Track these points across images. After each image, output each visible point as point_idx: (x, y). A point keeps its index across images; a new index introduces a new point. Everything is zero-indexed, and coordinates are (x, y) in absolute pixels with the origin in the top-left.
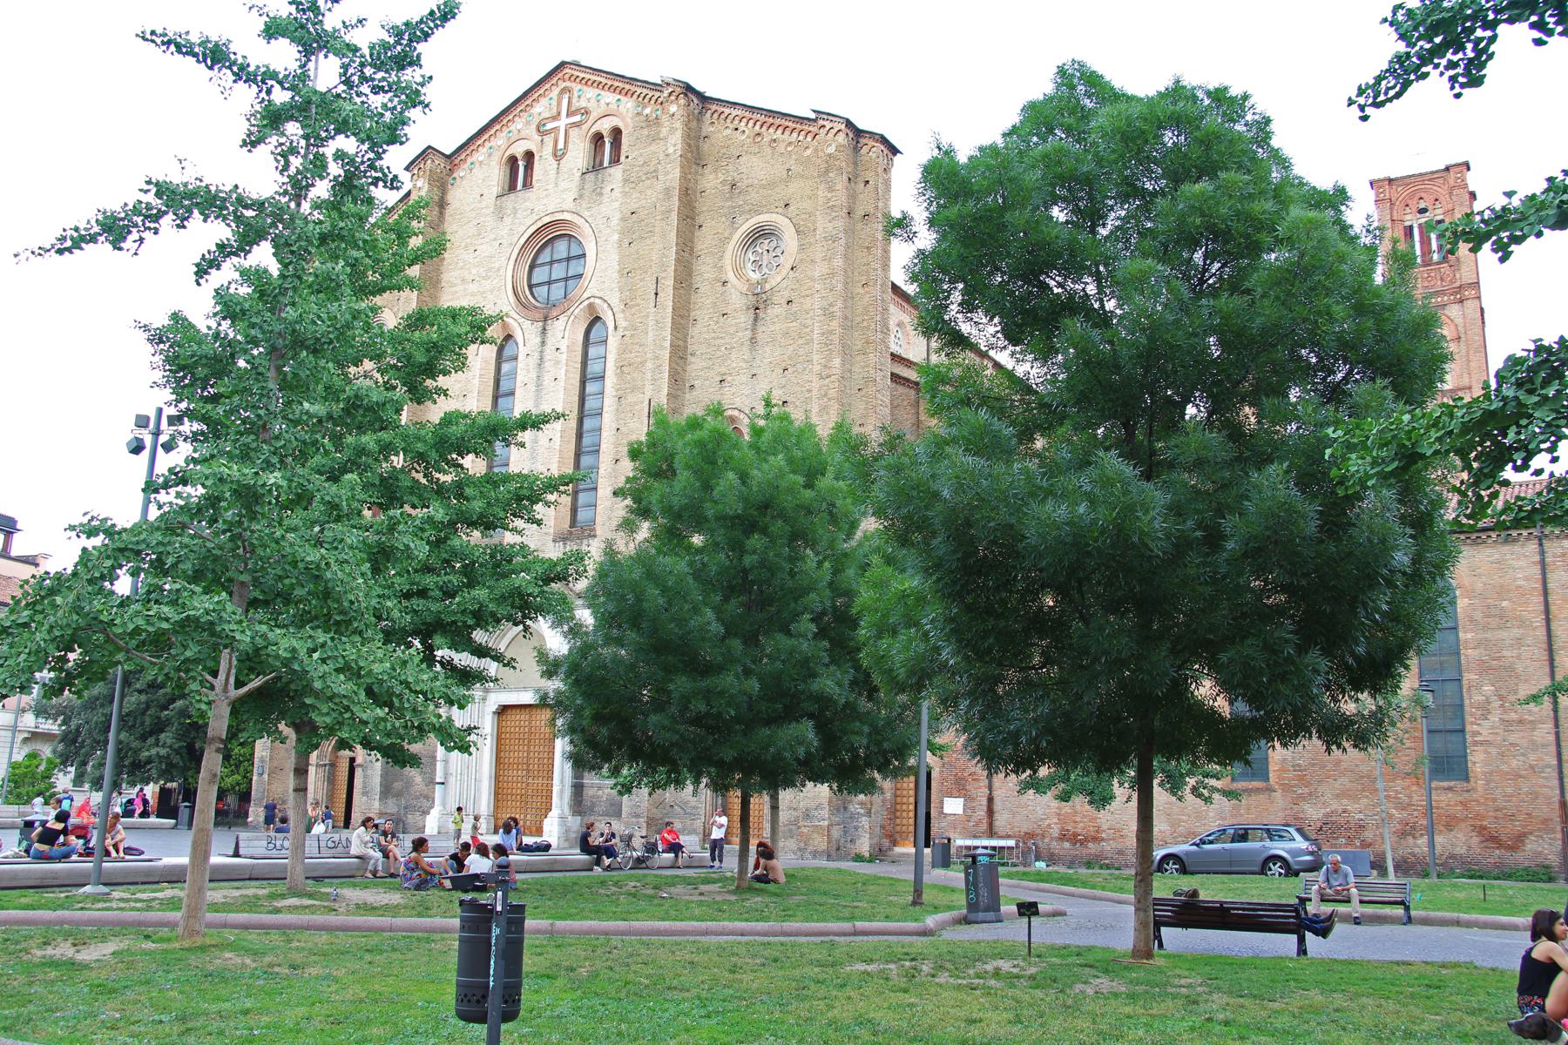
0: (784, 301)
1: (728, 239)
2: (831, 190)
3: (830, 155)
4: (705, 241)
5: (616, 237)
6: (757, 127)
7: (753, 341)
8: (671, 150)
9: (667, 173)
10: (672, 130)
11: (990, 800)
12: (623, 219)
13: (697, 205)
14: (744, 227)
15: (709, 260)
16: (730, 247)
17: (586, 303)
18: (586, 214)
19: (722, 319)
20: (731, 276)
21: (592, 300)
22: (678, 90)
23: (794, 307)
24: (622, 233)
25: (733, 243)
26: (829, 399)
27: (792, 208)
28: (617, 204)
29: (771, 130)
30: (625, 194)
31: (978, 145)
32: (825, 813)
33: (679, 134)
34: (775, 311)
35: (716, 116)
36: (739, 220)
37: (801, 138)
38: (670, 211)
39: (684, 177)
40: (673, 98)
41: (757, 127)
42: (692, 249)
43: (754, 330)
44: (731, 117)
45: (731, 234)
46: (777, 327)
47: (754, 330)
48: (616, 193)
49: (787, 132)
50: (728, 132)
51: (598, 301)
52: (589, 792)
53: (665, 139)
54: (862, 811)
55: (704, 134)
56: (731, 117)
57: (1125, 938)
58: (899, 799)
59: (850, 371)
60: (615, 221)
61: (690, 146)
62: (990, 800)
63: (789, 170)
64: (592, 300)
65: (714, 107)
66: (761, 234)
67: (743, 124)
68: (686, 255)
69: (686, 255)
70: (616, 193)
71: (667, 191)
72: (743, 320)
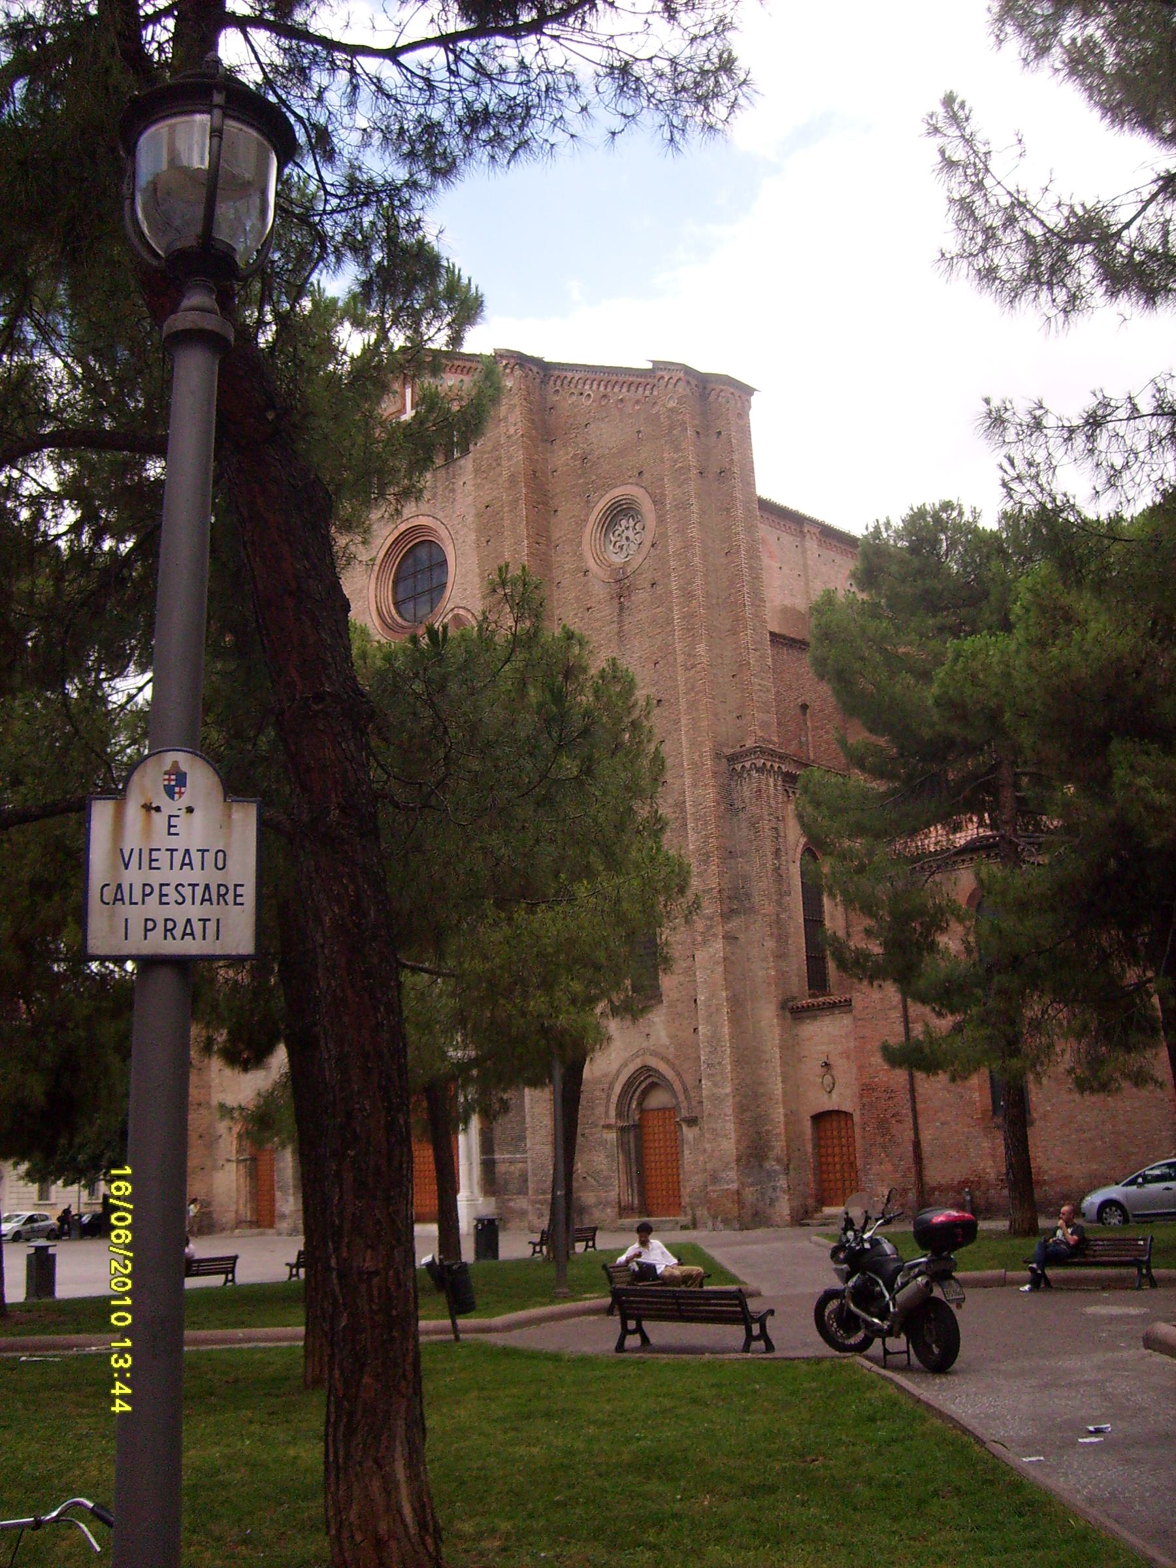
0: (647, 585)
1: (586, 521)
2: (677, 449)
3: (672, 410)
4: (561, 529)
5: (473, 536)
6: (602, 388)
7: (620, 634)
8: (512, 431)
9: (510, 458)
10: (512, 408)
11: (917, 1144)
12: (479, 515)
13: (549, 487)
14: (600, 505)
15: (568, 548)
16: (588, 530)
17: (450, 616)
18: (440, 515)
19: (587, 614)
20: (591, 564)
21: (456, 612)
22: (512, 361)
23: (659, 590)
24: (478, 531)
25: (590, 524)
26: (697, 693)
27: (645, 476)
28: (470, 499)
29: (616, 389)
30: (478, 487)
31: (526, 169)
32: (732, 1174)
33: (518, 410)
34: (641, 596)
35: (559, 383)
36: (594, 497)
37: (647, 393)
38: (518, 500)
39: (530, 459)
40: (508, 371)
41: (602, 388)
42: (548, 539)
43: (621, 622)
44: (574, 381)
45: (587, 515)
46: (643, 615)
47: (621, 622)
48: (469, 487)
49: (633, 388)
50: (574, 398)
51: (461, 612)
52: (501, 1168)
53: (506, 418)
54: (777, 1167)
55: (549, 405)
56: (574, 381)
57: (741, 1342)
58: (823, 1151)
59: (721, 656)
60: (470, 519)
61: (532, 421)
62: (917, 1144)
63: (639, 432)
64: (456, 612)
65: (556, 373)
66: (621, 511)
67: (587, 387)
68: (543, 547)
69: (543, 547)
70: (469, 487)
71: (513, 480)
72: (607, 612)
